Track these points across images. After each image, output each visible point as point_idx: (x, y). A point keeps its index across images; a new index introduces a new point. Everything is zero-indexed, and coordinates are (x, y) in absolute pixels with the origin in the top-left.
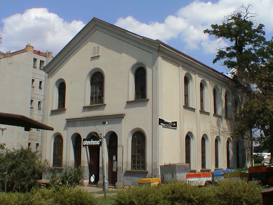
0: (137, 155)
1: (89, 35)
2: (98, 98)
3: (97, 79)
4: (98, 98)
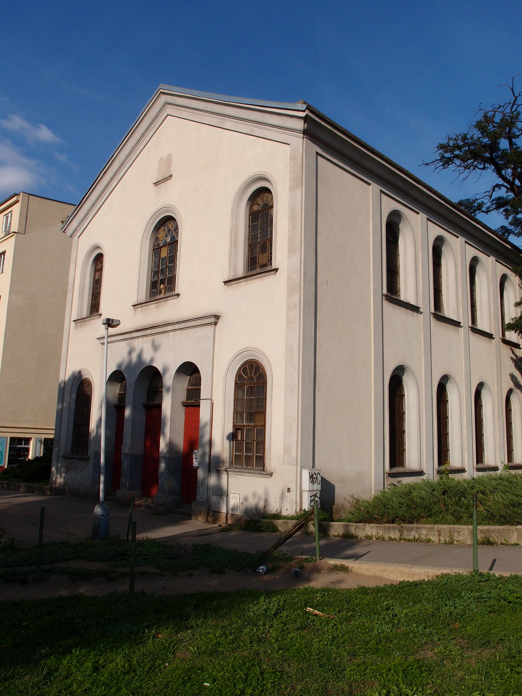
0: (245, 426)
1: (116, 182)
2: (162, 280)
3: (165, 233)
4: (162, 280)
